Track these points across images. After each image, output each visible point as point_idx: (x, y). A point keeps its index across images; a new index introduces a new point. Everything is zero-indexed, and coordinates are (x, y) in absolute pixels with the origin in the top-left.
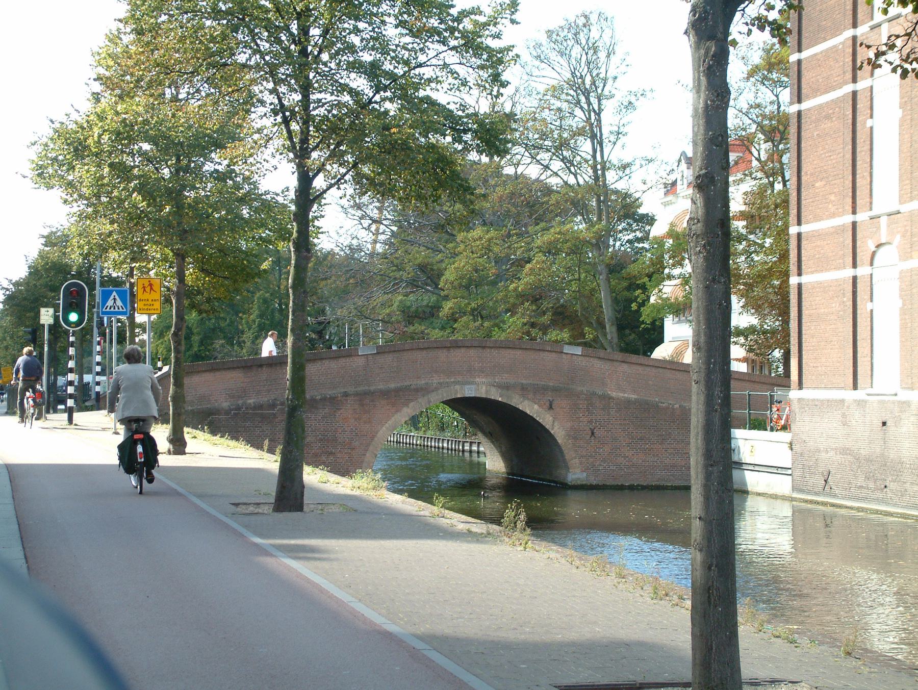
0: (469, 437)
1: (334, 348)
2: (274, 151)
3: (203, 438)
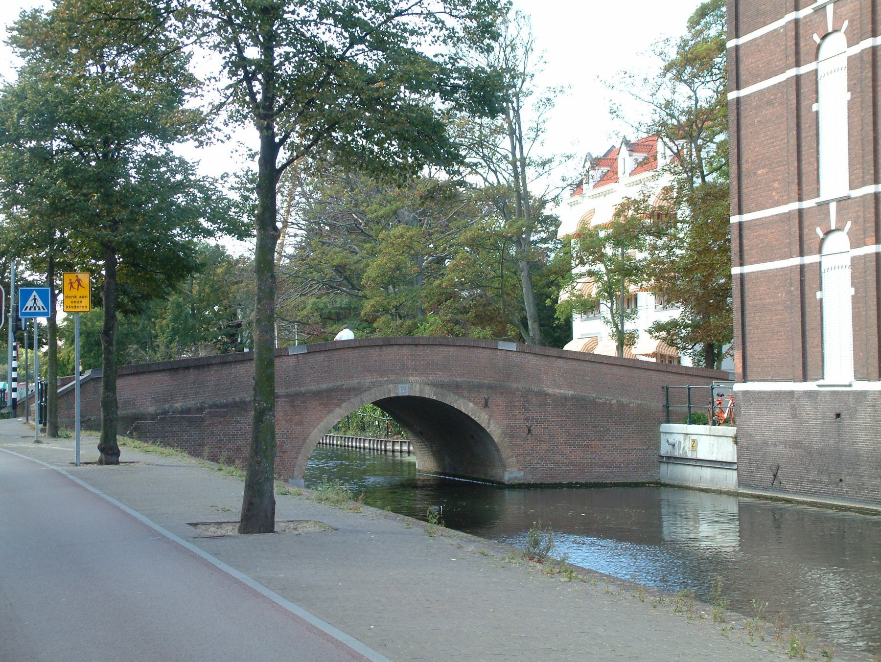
0: (392, 436)
1: (246, 350)
2: (226, 118)
3: (133, 445)
